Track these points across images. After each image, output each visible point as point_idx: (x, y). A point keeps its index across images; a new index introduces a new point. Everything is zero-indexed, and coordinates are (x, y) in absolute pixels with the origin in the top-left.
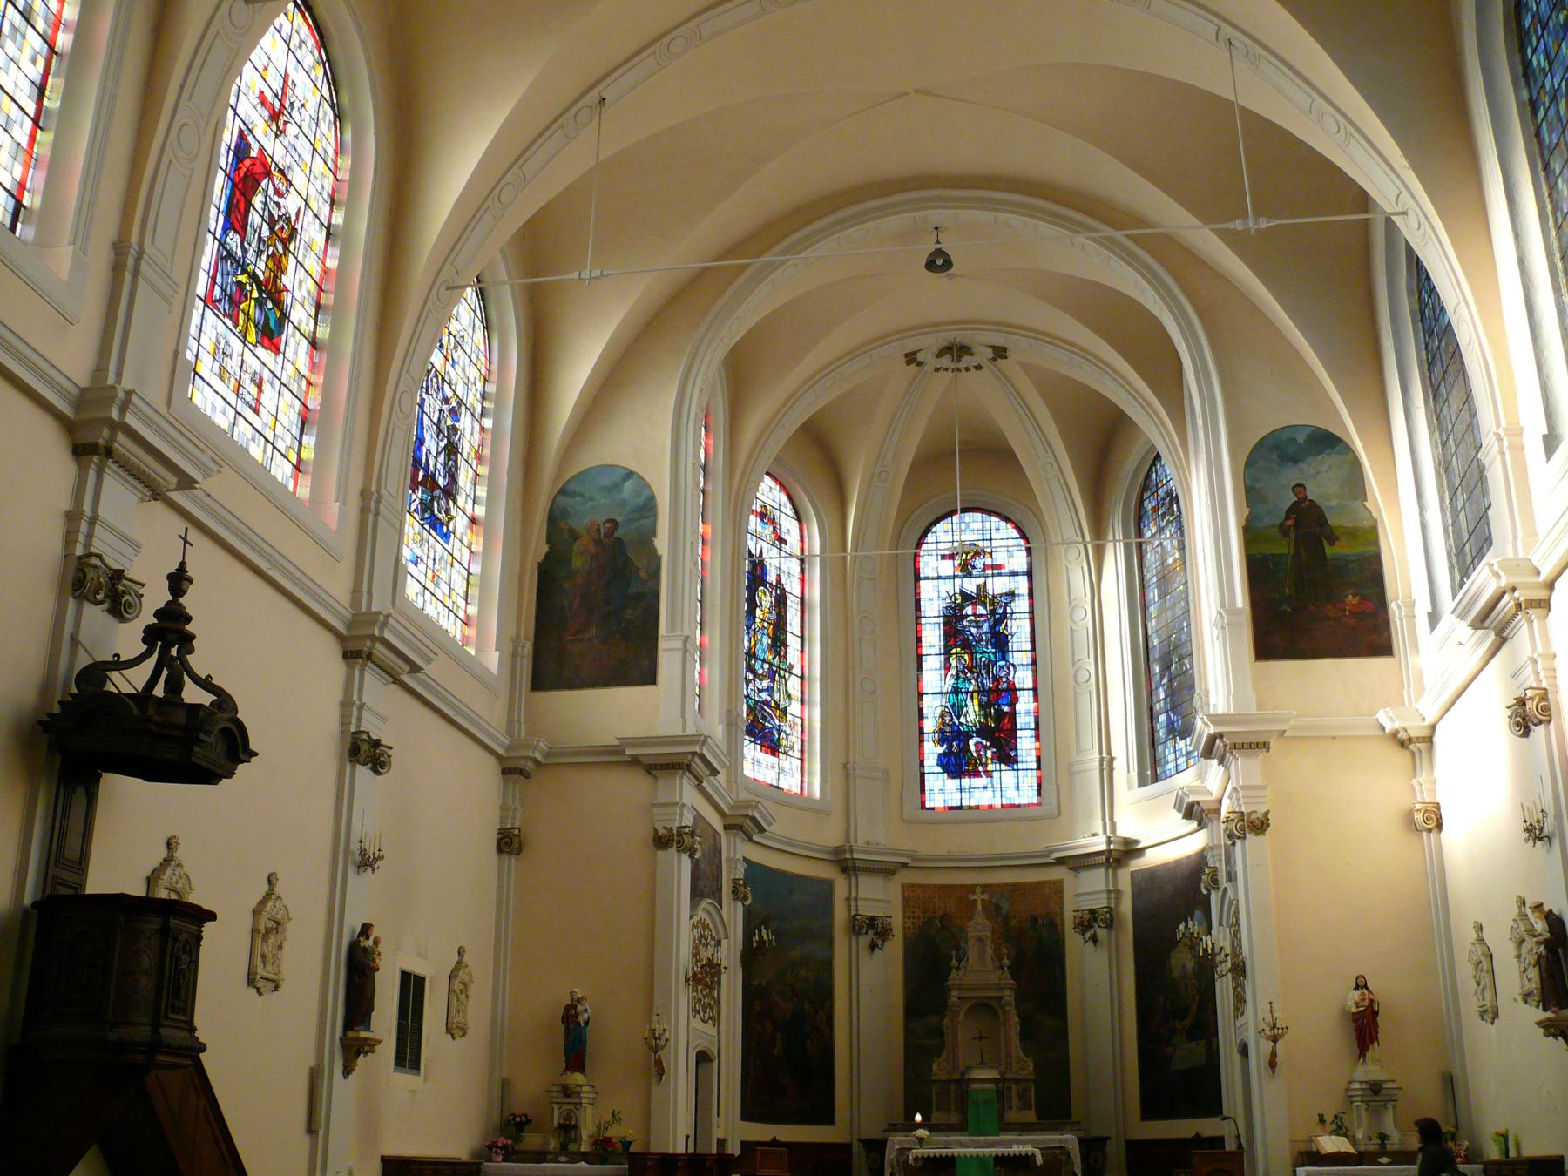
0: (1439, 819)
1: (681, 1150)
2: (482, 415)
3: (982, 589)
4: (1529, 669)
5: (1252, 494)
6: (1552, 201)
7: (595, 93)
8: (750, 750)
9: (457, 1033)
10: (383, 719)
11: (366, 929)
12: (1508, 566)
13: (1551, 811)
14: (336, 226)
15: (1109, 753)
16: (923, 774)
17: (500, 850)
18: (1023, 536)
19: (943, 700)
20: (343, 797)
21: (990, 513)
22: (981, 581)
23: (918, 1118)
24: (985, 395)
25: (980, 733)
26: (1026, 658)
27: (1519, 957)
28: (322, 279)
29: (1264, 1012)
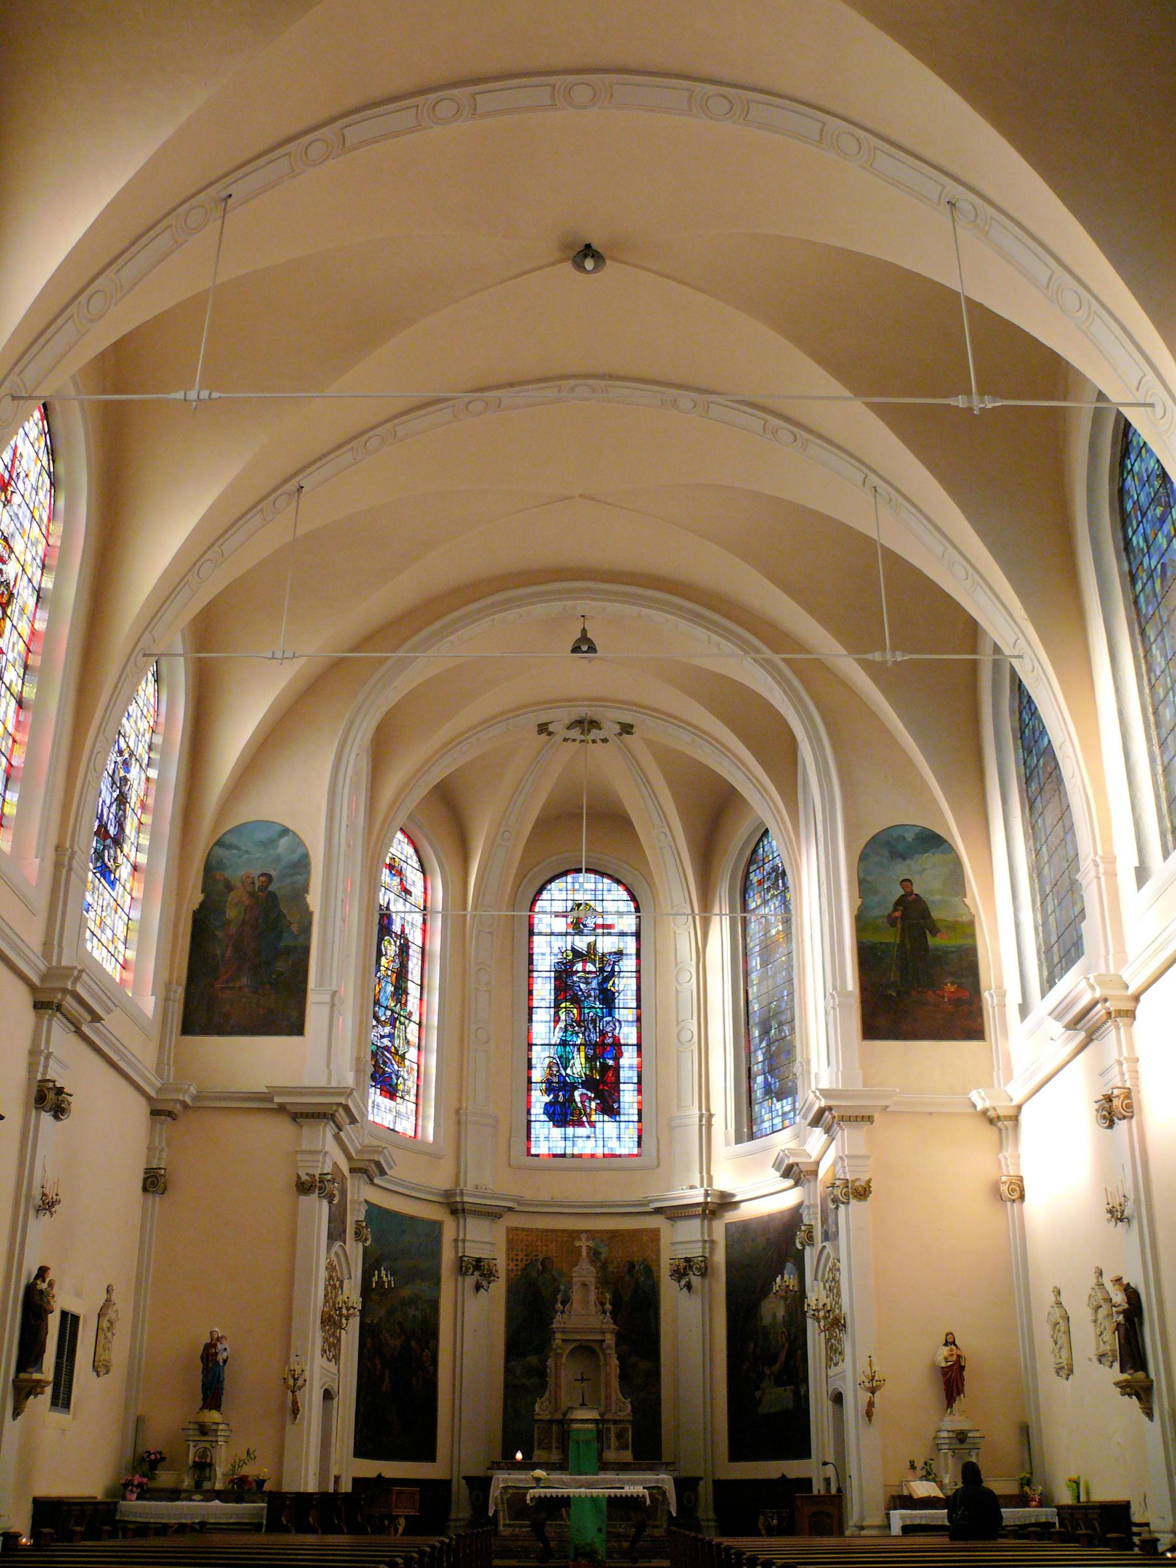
0: (1022, 1191)
1: (312, 1487)
2: (148, 765)
3: (592, 947)
4: (1116, 1069)
5: (864, 886)
6: (1146, 662)
7: (294, 481)
8: (375, 1095)
9: (102, 1370)
10: (65, 1066)
11: (42, 1272)
12: (1102, 980)
13: (1131, 1196)
14: (46, 590)
15: (708, 1109)
16: (529, 1122)
17: (145, 1189)
18: (633, 898)
19: (552, 1051)
20: (27, 1140)
21: (603, 875)
22: (591, 939)
23: (519, 1456)
24: (610, 768)
25: (585, 1085)
26: (630, 1015)
27: (1095, 1321)
28: (30, 639)
29: (863, 1365)
